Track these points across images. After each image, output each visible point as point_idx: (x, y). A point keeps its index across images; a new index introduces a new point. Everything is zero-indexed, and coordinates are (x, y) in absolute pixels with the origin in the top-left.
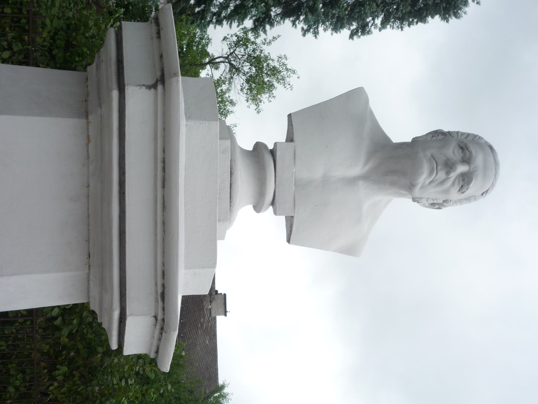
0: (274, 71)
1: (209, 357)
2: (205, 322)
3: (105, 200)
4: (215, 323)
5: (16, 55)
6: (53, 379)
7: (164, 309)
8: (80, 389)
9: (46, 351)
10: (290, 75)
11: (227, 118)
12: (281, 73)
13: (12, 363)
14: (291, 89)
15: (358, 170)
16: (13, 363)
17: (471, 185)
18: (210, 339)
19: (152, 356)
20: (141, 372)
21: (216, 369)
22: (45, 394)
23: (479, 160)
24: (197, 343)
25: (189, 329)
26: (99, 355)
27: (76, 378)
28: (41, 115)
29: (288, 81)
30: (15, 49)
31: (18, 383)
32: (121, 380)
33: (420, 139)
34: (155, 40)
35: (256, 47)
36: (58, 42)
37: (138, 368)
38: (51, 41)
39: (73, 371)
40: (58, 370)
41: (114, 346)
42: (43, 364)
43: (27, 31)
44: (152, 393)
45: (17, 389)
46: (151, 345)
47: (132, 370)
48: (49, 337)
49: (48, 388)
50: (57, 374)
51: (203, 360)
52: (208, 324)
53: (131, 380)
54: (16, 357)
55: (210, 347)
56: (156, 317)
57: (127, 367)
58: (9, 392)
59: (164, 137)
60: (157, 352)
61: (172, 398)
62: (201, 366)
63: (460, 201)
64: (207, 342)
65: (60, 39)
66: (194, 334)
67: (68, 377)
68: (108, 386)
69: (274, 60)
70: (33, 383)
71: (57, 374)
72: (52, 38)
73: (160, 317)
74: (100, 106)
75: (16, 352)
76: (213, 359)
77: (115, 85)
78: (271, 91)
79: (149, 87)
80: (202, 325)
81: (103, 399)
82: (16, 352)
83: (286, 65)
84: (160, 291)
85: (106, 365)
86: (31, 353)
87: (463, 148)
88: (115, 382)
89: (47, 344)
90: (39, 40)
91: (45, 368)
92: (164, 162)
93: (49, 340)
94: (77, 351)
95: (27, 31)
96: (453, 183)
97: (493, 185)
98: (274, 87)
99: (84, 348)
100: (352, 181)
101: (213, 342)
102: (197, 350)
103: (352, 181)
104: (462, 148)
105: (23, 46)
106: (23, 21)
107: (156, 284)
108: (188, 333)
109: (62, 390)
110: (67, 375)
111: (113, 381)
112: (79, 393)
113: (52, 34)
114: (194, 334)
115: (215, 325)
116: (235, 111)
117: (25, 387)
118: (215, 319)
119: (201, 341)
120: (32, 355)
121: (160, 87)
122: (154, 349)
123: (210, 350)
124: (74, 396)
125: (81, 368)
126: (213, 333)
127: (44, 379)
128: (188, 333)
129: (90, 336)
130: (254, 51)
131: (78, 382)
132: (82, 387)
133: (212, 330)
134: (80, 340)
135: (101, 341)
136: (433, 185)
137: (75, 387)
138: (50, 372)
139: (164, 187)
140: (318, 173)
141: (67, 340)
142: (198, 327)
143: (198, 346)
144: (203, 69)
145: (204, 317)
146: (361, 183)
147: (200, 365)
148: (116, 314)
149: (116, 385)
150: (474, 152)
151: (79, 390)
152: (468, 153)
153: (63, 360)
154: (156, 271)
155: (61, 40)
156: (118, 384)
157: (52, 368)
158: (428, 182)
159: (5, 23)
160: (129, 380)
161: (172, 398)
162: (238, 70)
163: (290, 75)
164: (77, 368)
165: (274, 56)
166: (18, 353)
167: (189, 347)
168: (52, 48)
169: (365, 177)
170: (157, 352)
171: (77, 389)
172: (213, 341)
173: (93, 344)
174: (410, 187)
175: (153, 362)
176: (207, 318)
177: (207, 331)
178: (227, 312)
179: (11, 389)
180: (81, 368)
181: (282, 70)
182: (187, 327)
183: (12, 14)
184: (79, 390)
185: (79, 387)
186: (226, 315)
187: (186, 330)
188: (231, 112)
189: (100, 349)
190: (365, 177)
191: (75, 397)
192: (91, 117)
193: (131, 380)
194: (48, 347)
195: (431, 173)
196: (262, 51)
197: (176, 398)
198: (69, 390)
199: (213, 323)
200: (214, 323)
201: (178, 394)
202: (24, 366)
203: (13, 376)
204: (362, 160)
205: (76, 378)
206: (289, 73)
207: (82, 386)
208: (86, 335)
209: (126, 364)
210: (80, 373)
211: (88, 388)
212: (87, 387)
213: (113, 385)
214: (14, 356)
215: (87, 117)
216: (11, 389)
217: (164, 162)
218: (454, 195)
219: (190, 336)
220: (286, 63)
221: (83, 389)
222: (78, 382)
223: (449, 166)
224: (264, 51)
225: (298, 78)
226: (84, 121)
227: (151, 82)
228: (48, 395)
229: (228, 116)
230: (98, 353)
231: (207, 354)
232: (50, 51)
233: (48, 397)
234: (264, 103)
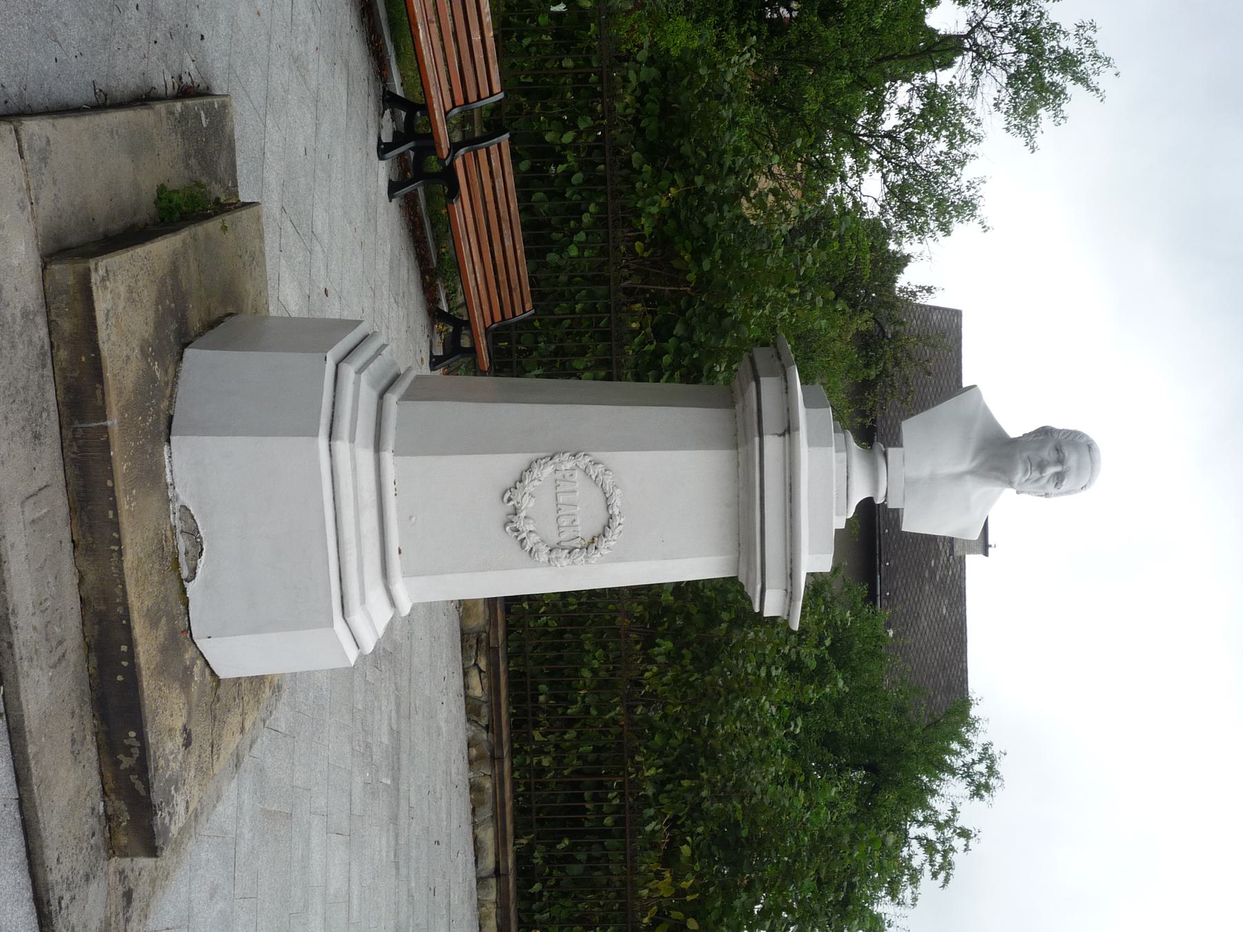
0: (1067, 62)
1: (948, 642)
2: (940, 566)
3: (750, 508)
4: (963, 569)
5: (584, 136)
6: (650, 660)
7: (792, 585)
8: (694, 678)
9: (638, 615)
10: (1098, 68)
11: (965, 167)
12: (1080, 66)
13: (587, 633)
14: (1102, 100)
15: (965, 466)
16: (588, 633)
17: (1064, 483)
18: (951, 605)
19: (785, 618)
20: (794, 657)
21: (964, 671)
22: (638, 684)
23: (1072, 459)
24: (920, 612)
25: (904, 581)
26: (724, 626)
27: (687, 661)
28: (706, 448)
29: (1095, 83)
30: (582, 126)
31: (596, 664)
32: (759, 667)
33: (1023, 439)
34: (784, 395)
35: (1030, 9)
36: (649, 105)
37: (788, 648)
38: (638, 105)
39: (682, 648)
40: (659, 646)
41: (757, 610)
42: (634, 636)
43: (601, 95)
44: (810, 691)
45: (594, 672)
46: (784, 609)
47: (779, 651)
48: (643, 592)
49: (642, 675)
50: (656, 653)
51: (935, 649)
52: (946, 571)
53: (777, 669)
54: (593, 622)
55: (950, 622)
56: (786, 590)
57: (769, 647)
58: (583, 677)
59: (790, 454)
60: (788, 615)
61: (860, 719)
62: (928, 661)
63: (1057, 495)
64: (944, 612)
65: (653, 101)
66: (914, 593)
67: (674, 657)
68: (738, 676)
69: (1069, 34)
70: (618, 665)
71: (656, 653)
72: (639, 100)
73: (789, 591)
74: (746, 443)
75: (592, 615)
76: (956, 647)
77: (756, 433)
78: (1060, 105)
79: (780, 435)
80: (933, 573)
81: (730, 697)
82: (592, 615)
83: (1093, 43)
84: (789, 573)
85: (734, 641)
86: (614, 618)
87: (1058, 450)
88: (749, 671)
89: (639, 605)
90: (619, 106)
91: (637, 642)
92: (791, 485)
93: (643, 597)
94: (688, 617)
95: (601, 95)
96: (1048, 481)
97: (1090, 481)
98: (1066, 95)
99: (698, 612)
100: (959, 477)
101: (958, 611)
102: (921, 628)
103: (959, 477)
104: (1057, 450)
105: (594, 120)
106: (593, 78)
107: (786, 568)
108: (902, 590)
109: (664, 679)
110: (672, 655)
111: (746, 668)
112: (691, 685)
113: (638, 93)
114: (914, 593)
115: (962, 574)
116: (979, 156)
117: (607, 670)
118: (962, 561)
119: (930, 609)
120: (617, 621)
121: (787, 436)
122: (786, 613)
123: (950, 628)
124: (683, 690)
125: (695, 645)
126: (957, 592)
127: (636, 660)
128: (902, 590)
129: (709, 593)
130: (1024, 14)
131: (691, 667)
132: (696, 675)
133: (955, 585)
134: (692, 600)
135: (727, 602)
136: (1029, 482)
137: (685, 675)
138: (644, 649)
139: (791, 502)
140: (925, 471)
141: (672, 598)
142: (924, 576)
143: (923, 618)
144: (933, 7)
145: (937, 557)
146: (968, 477)
147: (926, 660)
148: (759, 587)
149: (750, 674)
150: (1067, 454)
151: (691, 679)
152: (1061, 455)
153: (666, 630)
154: (786, 559)
155: (654, 102)
156: (754, 674)
157: (649, 642)
158: (1024, 479)
159: (565, 84)
160: (773, 668)
161: (860, 719)
162: (992, 59)
163: (1098, 68)
164: (688, 645)
165: (1068, 25)
166: (595, 616)
167: (903, 620)
168: (640, 116)
169: (972, 472)
170: (788, 615)
171: (688, 677)
172: (958, 608)
173: (713, 607)
174: (1010, 484)
175: (786, 622)
176: (943, 558)
177: (944, 588)
178: (991, 546)
179: (586, 673)
180: (695, 645)
181: (1083, 60)
182: (898, 576)
183: (574, 68)
184: (691, 679)
185: (692, 676)
186: (986, 554)
187: (897, 584)
188: (973, 156)
189: (725, 616)
190: (972, 472)
191: (685, 692)
192: (740, 450)
193: (777, 669)
194: (641, 608)
195: (1026, 472)
196: (1042, 14)
197: (868, 720)
198: (675, 680)
199: (959, 569)
200: (961, 569)
201: (872, 711)
202: (604, 637)
203: (589, 652)
204: (969, 456)
205: (687, 661)
206: (1098, 64)
207: (696, 674)
208: (703, 591)
209: (769, 642)
210: (693, 652)
211: (706, 678)
212: (704, 676)
213: (747, 674)
214: (590, 621)
215: (737, 448)
216: (586, 673)
217: (791, 485)
218: (1051, 488)
219: (905, 597)
220: (1094, 37)
221: (697, 679)
222: (691, 667)
223: (1041, 467)
224: (1046, 13)
225: (1117, 75)
226: (734, 452)
227: (781, 431)
228: (641, 686)
229: (968, 163)
230: (722, 621)
231: (944, 637)
232: (636, 121)
233: (643, 689)
234: (1042, 132)
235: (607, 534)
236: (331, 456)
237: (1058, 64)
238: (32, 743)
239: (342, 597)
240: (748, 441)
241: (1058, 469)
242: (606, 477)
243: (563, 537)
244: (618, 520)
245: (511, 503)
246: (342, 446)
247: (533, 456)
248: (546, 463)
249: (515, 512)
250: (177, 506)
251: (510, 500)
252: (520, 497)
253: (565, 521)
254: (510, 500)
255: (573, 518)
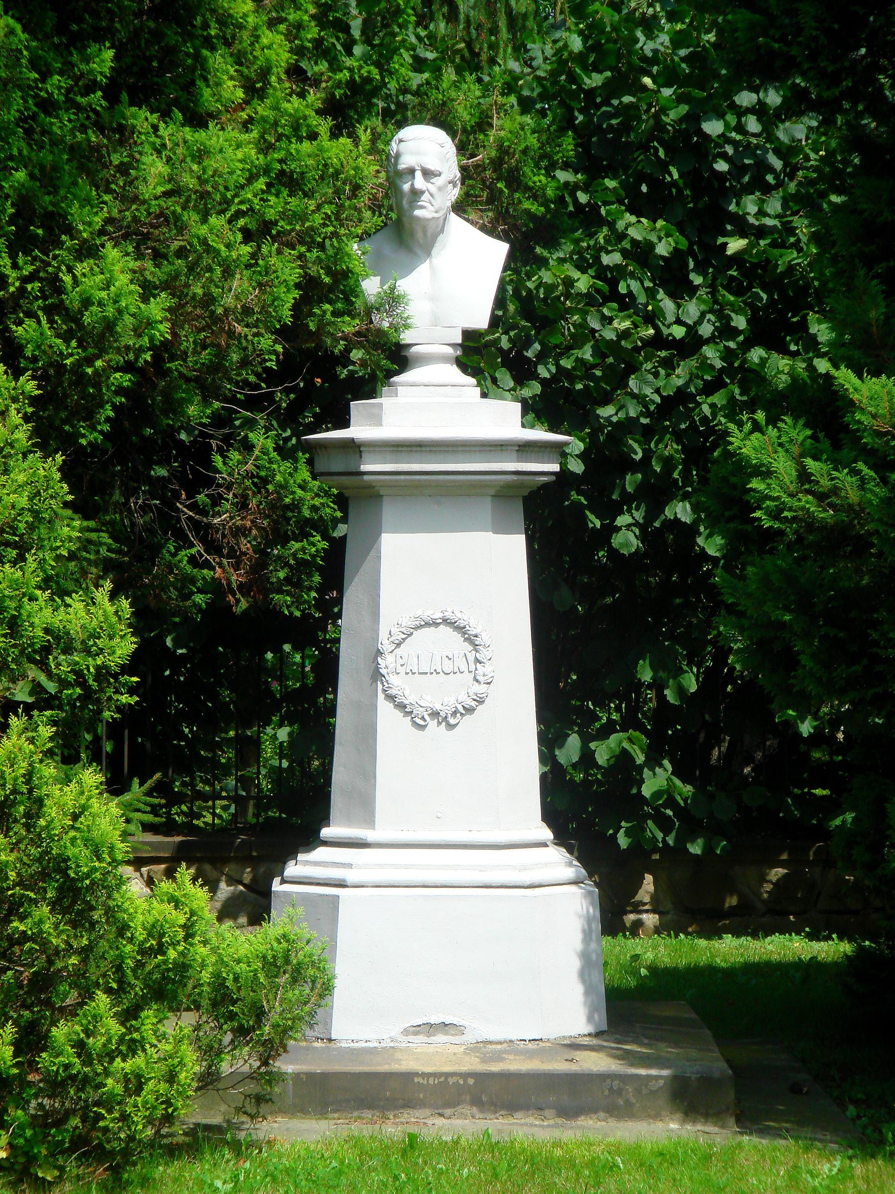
41: (553, 478)
226: (385, 498)
235: (462, 625)
236: (363, 887)
237: (783, 421)
238: (844, 1174)
239: (473, 887)
240: (370, 486)
241: (418, 174)
242: (404, 625)
243: (464, 668)
244: (448, 615)
245: (427, 717)
246: (350, 876)
247: (381, 696)
248: (387, 681)
249: (435, 714)
250: (402, 1038)
251: (423, 718)
252: (421, 709)
253: (448, 666)
254: (423, 718)
255: (444, 658)
